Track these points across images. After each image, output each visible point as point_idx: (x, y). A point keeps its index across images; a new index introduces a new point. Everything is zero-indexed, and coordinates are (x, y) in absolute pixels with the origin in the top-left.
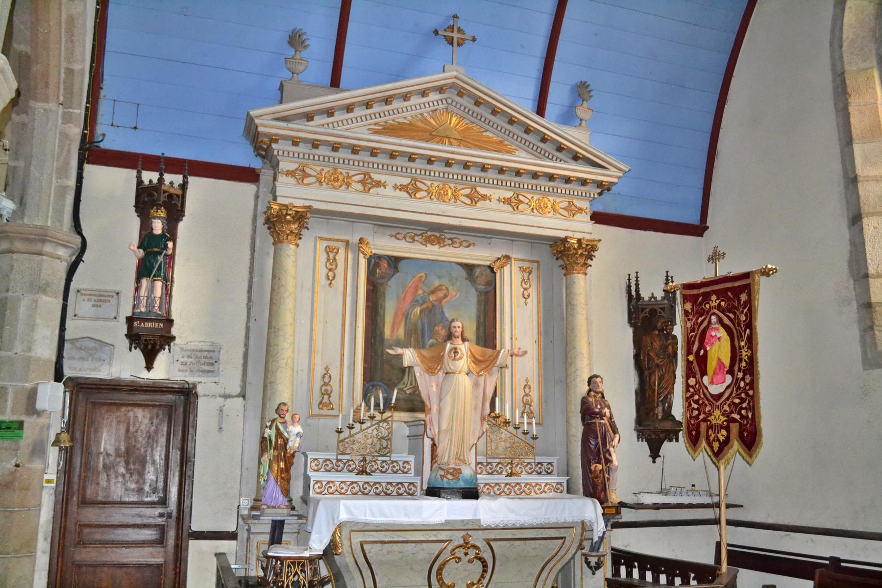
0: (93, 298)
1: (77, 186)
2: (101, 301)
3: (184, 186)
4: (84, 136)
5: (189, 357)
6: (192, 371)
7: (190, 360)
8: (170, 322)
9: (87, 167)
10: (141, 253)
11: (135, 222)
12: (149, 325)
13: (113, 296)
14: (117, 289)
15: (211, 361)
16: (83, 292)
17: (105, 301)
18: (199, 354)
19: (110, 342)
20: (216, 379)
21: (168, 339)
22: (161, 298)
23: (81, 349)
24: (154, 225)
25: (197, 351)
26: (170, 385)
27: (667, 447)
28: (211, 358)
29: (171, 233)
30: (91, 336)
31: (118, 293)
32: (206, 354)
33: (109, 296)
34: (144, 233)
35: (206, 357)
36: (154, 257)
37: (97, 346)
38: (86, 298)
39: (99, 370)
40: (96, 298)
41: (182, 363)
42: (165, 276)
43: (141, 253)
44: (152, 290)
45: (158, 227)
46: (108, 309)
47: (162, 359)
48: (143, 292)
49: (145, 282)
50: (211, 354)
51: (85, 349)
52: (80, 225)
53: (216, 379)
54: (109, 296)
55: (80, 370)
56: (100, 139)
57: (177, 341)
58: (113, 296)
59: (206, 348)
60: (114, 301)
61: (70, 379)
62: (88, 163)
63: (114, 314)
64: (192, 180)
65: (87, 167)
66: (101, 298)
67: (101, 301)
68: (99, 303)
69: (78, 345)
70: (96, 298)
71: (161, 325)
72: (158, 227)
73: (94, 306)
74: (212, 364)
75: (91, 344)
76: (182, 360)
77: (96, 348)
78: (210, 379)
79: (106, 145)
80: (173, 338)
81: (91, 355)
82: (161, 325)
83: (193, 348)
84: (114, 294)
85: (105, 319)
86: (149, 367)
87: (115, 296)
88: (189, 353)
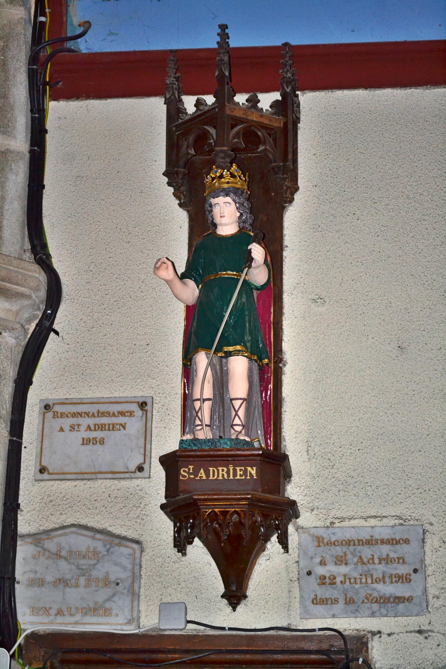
0: (85, 422)
1: (31, 152)
2: (102, 427)
3: (287, 108)
4: (38, 30)
5: (341, 560)
6: (349, 601)
7: (343, 569)
8: (275, 463)
9: (55, 109)
10: (191, 291)
11: (180, 220)
12: (220, 473)
13: (131, 414)
14: (140, 393)
15: (402, 570)
16: (57, 408)
17: (112, 427)
18: (366, 552)
19: (130, 534)
20: (421, 621)
21: (277, 514)
22: (248, 400)
23: (58, 555)
24: (216, 211)
25: (361, 542)
26: (293, 646)
27: (189, 548)
28: (402, 560)
29: (265, 224)
30: (83, 522)
31: (143, 405)
32: (385, 550)
33: (122, 414)
34: (195, 243)
35: (387, 560)
36: (231, 311)
37: (99, 546)
38: (67, 422)
39: (107, 612)
40: (91, 421)
41: (322, 580)
42: (255, 342)
43: (191, 291)
44: (221, 382)
45: (227, 216)
46: (120, 449)
47: (270, 564)
48: (204, 388)
49: (202, 360)
50: (403, 549)
51: (72, 555)
52: (44, 246)
53: (421, 621)
54: (122, 414)
55: (60, 613)
56: (79, 31)
57: (306, 519)
58: (131, 414)
59: (386, 534)
60: (134, 425)
61: (34, 637)
62: (55, 98)
63: (139, 460)
64: (307, 100)
65: (55, 109)
66: (103, 419)
67: (102, 427)
68: (98, 434)
69: (51, 545)
70: (91, 421)
71: (253, 471)
72: (227, 216)
73: (86, 442)
74: (404, 579)
75: (82, 542)
76: (321, 571)
77: (95, 553)
78: (403, 620)
79: (90, 45)
80: (290, 509)
81: (83, 572)
82: (253, 471)
83: (348, 535)
84: (135, 408)
85: (115, 474)
86: (235, 595)
87: (138, 413)
88: (339, 550)
